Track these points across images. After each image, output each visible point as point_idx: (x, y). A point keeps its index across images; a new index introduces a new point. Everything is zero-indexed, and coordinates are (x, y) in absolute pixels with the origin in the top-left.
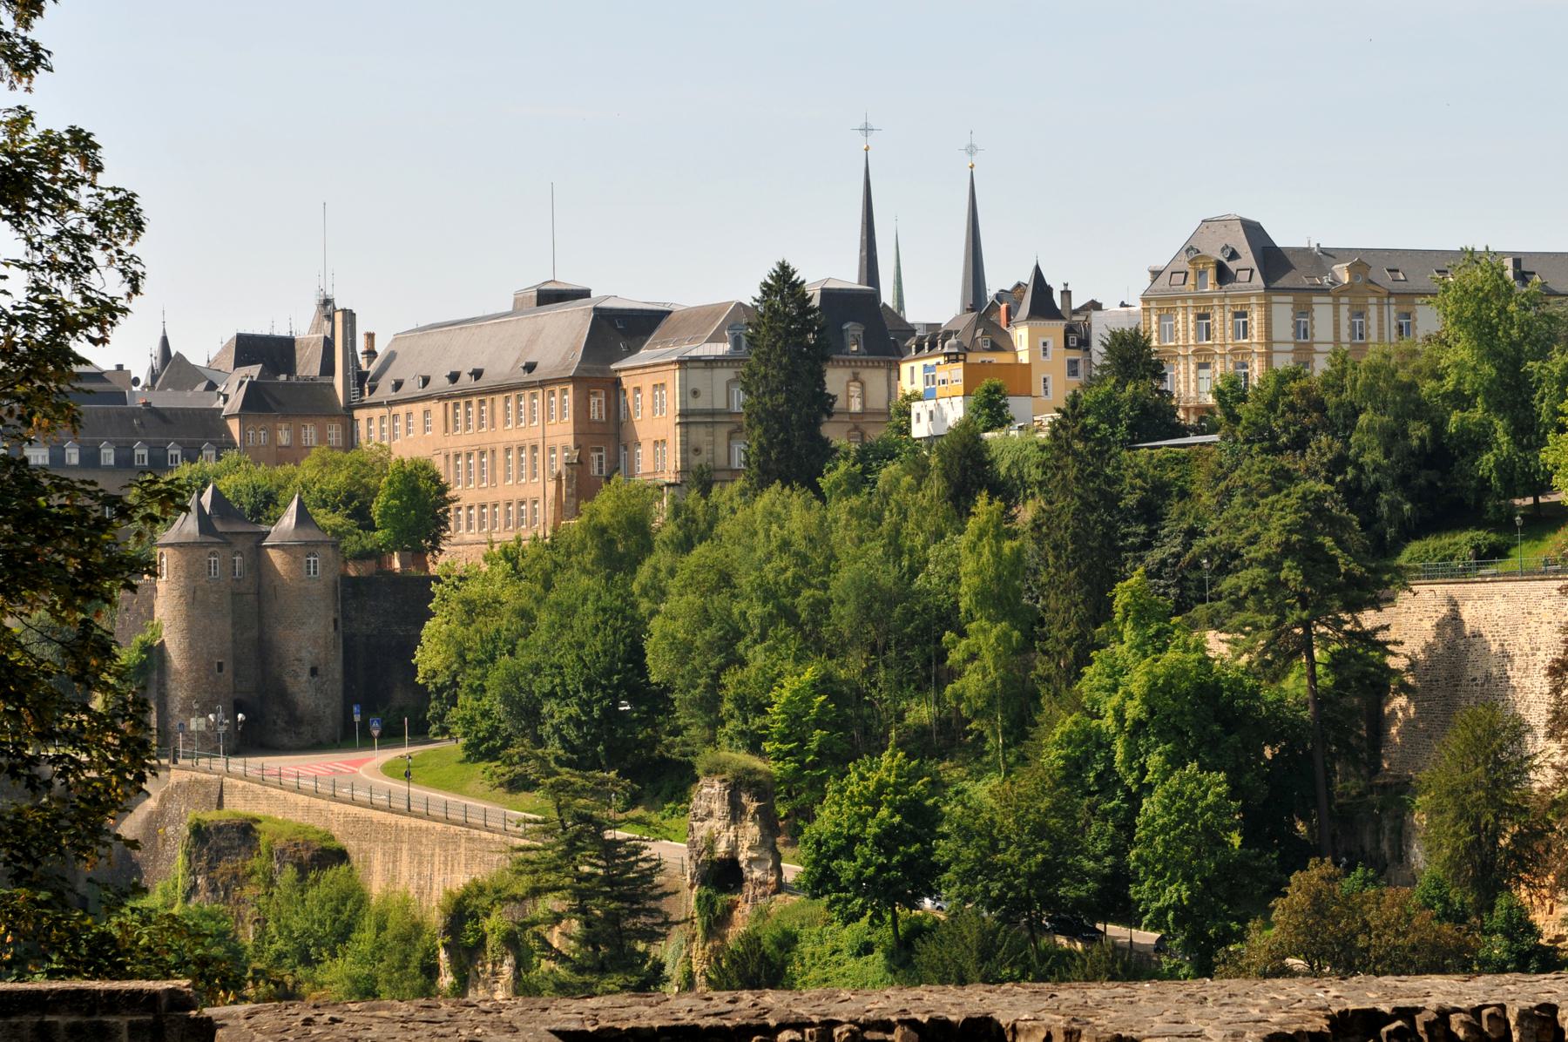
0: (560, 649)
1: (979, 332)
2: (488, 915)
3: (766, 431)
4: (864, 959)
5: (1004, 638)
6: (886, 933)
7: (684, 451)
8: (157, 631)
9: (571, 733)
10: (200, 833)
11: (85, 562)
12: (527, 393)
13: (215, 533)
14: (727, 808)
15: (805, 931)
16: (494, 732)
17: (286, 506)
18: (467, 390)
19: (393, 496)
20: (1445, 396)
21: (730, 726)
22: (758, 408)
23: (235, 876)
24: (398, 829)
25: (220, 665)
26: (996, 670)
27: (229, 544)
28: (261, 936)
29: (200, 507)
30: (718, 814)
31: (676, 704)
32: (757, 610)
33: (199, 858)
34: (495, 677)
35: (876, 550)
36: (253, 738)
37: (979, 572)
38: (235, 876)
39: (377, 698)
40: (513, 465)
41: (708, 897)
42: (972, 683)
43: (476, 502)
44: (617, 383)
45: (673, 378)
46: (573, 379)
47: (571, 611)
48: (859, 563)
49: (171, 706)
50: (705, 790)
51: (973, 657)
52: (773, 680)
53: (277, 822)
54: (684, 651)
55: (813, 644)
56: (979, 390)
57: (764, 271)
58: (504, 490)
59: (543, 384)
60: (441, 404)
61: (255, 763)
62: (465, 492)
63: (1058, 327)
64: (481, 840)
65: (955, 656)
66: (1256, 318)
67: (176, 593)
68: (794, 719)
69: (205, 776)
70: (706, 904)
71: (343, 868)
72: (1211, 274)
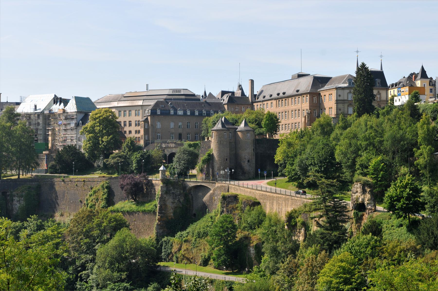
0: (310, 154)
1: (408, 82)
2: (298, 218)
3: (359, 103)
4: (401, 228)
5: (430, 150)
6: (407, 221)
10: (224, 198)
11: (100, 230)
12: (297, 97)
13: (225, 127)
14: (362, 190)
15: (384, 221)
16: (296, 174)
17: (241, 123)
18: (282, 98)
19: (267, 120)
21: (358, 172)
22: (357, 98)
23: (233, 208)
25: (227, 159)
26: (427, 158)
27: (229, 130)
28: (240, 223)
29: (222, 121)
30: (359, 192)
31: (343, 167)
32: (364, 143)
33: (224, 204)
34: (297, 160)
35: (395, 128)
36: (234, 177)
38: (233, 208)
40: (294, 114)
41: (357, 213)
42: (421, 161)
43: (284, 124)
44: (319, 94)
45: (334, 92)
47: (316, 144)
48: (389, 131)
49: (215, 169)
50: (356, 186)
52: (369, 160)
55: (378, 152)
56: (413, 93)
58: (292, 120)
60: (275, 101)
61: (236, 182)
62: (283, 121)
63: (428, 81)
64: (295, 199)
65: (416, 154)
69: (224, 185)
70: (356, 215)
71: (259, 206)
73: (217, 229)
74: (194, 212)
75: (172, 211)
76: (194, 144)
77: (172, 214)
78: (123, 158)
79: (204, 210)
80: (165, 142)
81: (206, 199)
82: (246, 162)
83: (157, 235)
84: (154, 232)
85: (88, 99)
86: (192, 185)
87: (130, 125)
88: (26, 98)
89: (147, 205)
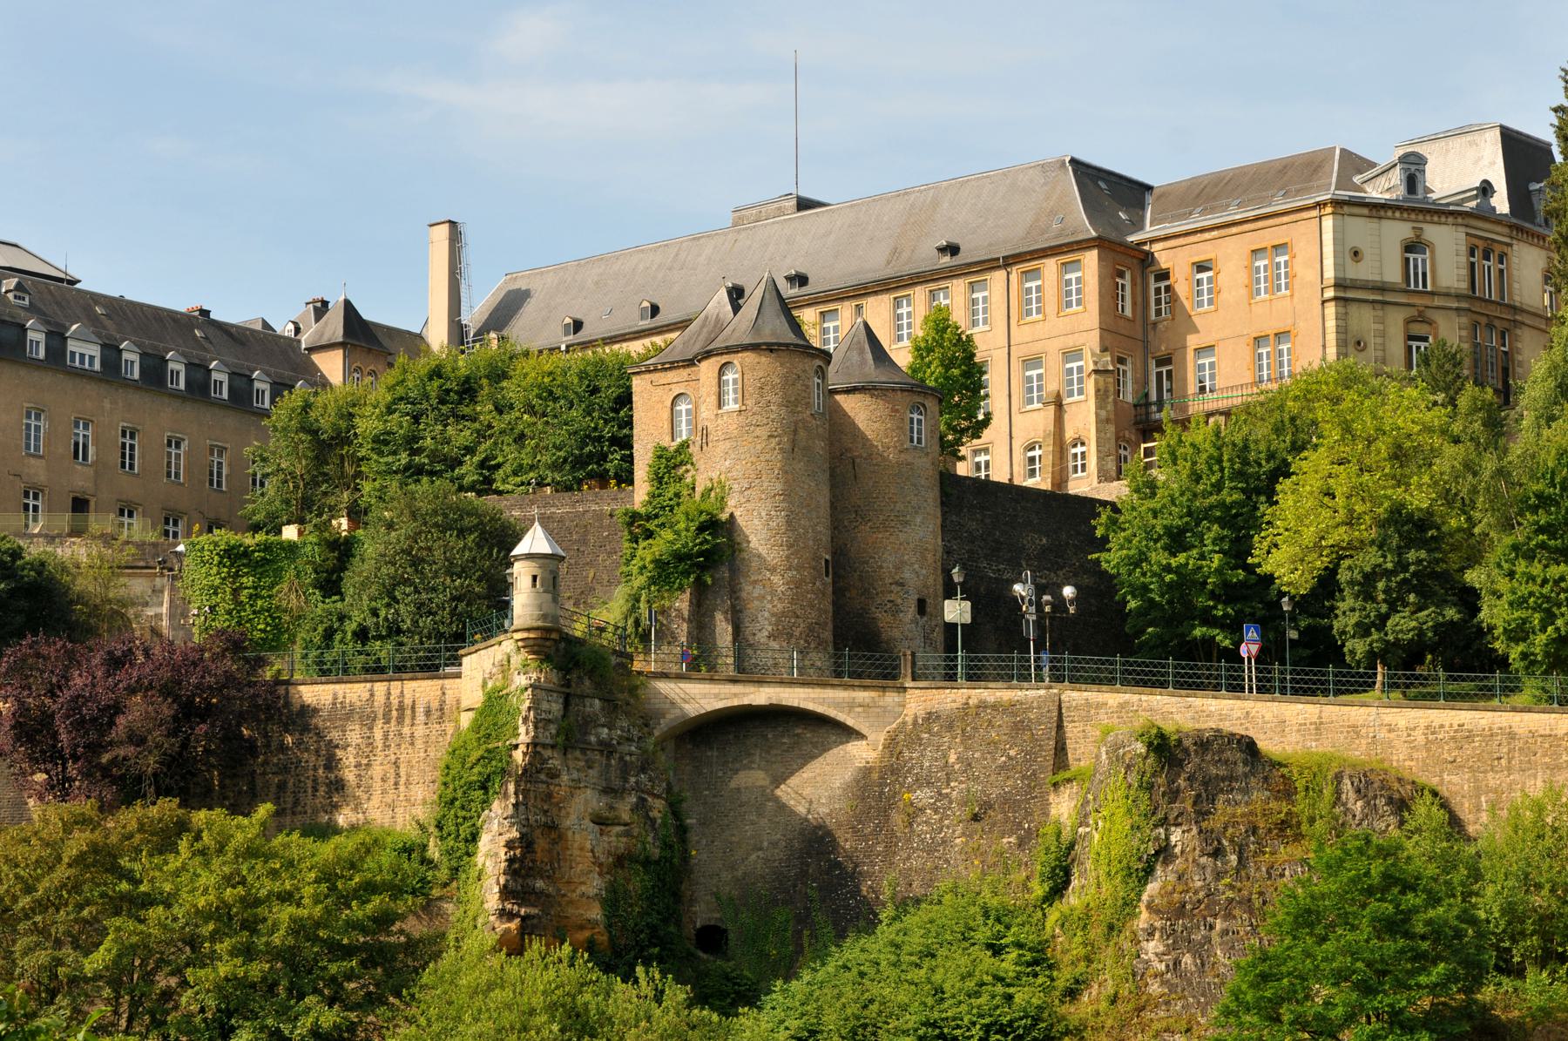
33: (1174, 795)
67: (763, 432)
75: (594, 884)
77: (596, 913)
82: (911, 611)
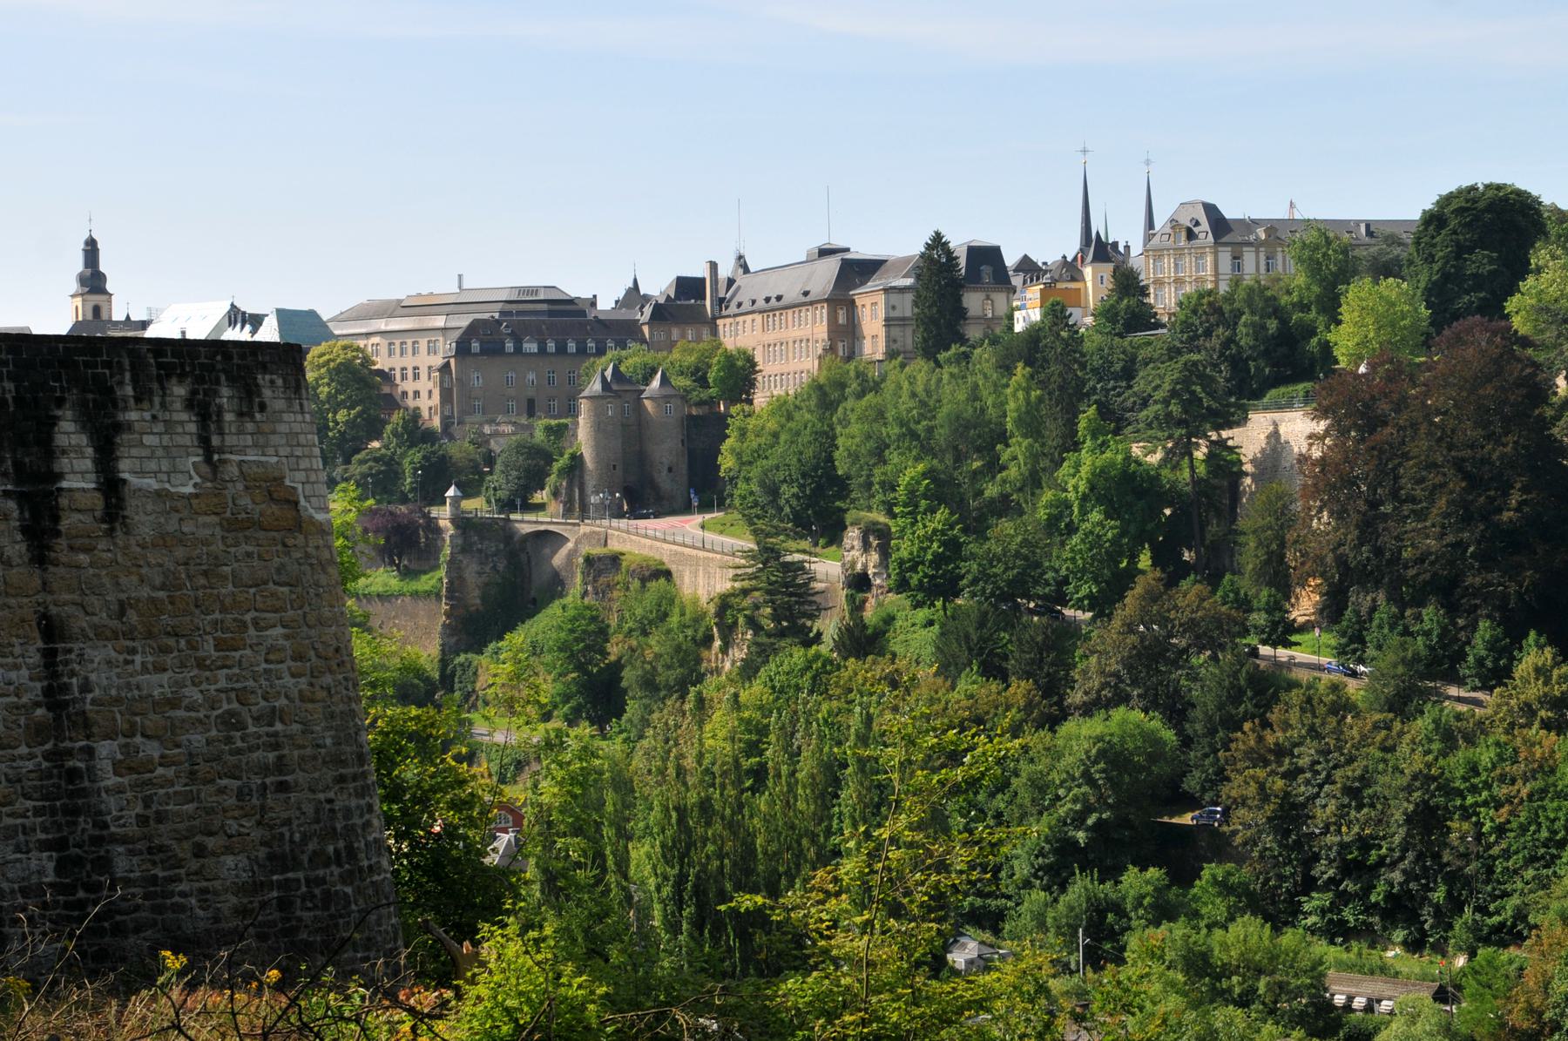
7: (887, 342)
8: (579, 448)
9: (794, 502)
10: (589, 561)
18: (775, 307)
20: (1294, 305)
24: (698, 558)
28: (622, 619)
37: (1017, 410)
39: (703, 489)
42: (1013, 472)
45: (881, 298)
46: (826, 300)
47: (798, 434)
51: (1015, 458)
53: (22, 513)
54: (854, 456)
55: (926, 450)
56: (1048, 304)
57: (927, 236)
59: (811, 303)
66: (1209, 259)
68: (912, 493)
70: (851, 599)
72: (1184, 235)
73: (563, 635)
74: (533, 594)
75: (477, 593)
76: (558, 425)
77: (478, 601)
78: (385, 464)
79: (555, 586)
80: (492, 422)
81: (558, 560)
82: (665, 472)
83: (443, 651)
84: (438, 641)
85: (312, 314)
86: (526, 529)
87: (416, 377)
88: (162, 311)
89: (424, 578)
